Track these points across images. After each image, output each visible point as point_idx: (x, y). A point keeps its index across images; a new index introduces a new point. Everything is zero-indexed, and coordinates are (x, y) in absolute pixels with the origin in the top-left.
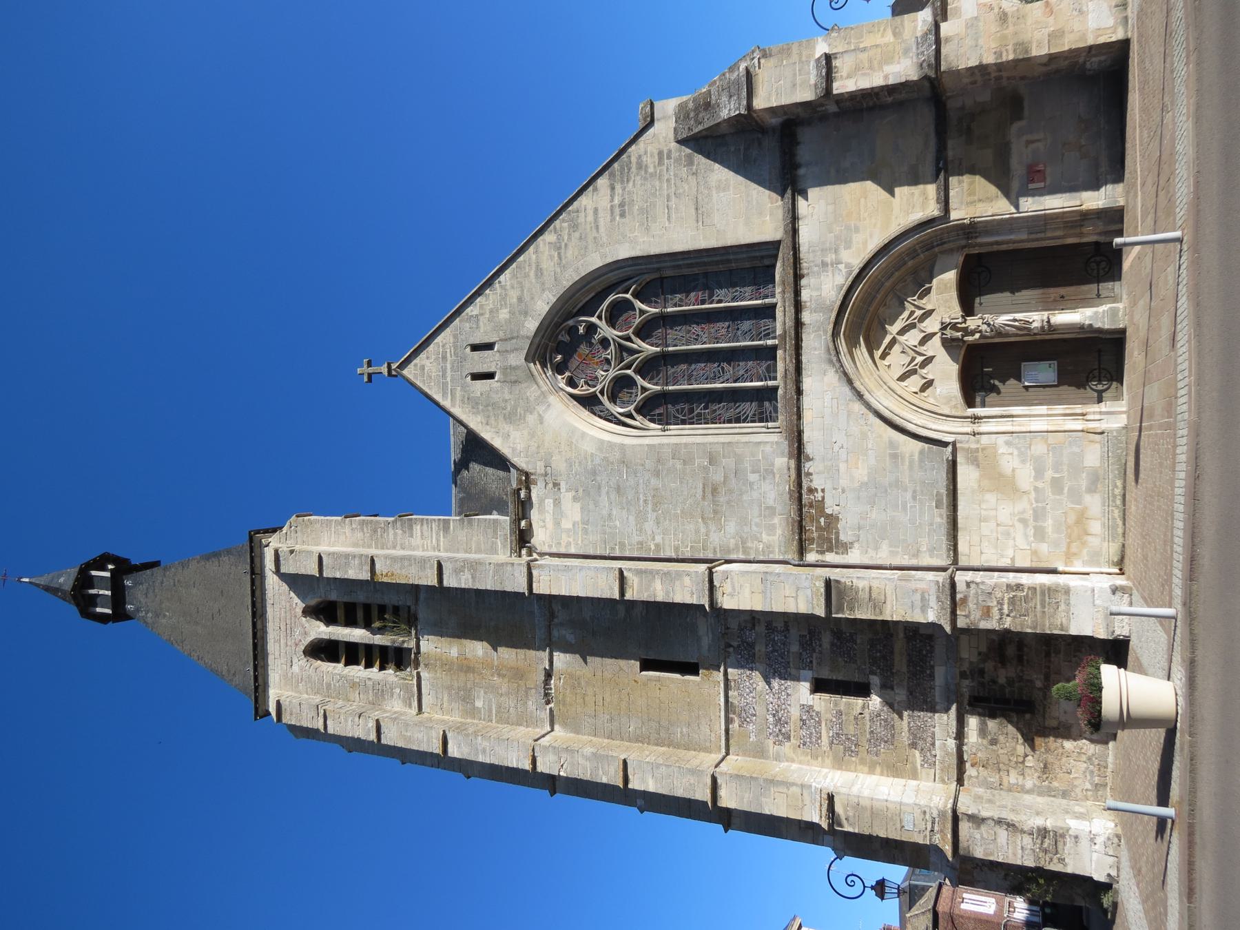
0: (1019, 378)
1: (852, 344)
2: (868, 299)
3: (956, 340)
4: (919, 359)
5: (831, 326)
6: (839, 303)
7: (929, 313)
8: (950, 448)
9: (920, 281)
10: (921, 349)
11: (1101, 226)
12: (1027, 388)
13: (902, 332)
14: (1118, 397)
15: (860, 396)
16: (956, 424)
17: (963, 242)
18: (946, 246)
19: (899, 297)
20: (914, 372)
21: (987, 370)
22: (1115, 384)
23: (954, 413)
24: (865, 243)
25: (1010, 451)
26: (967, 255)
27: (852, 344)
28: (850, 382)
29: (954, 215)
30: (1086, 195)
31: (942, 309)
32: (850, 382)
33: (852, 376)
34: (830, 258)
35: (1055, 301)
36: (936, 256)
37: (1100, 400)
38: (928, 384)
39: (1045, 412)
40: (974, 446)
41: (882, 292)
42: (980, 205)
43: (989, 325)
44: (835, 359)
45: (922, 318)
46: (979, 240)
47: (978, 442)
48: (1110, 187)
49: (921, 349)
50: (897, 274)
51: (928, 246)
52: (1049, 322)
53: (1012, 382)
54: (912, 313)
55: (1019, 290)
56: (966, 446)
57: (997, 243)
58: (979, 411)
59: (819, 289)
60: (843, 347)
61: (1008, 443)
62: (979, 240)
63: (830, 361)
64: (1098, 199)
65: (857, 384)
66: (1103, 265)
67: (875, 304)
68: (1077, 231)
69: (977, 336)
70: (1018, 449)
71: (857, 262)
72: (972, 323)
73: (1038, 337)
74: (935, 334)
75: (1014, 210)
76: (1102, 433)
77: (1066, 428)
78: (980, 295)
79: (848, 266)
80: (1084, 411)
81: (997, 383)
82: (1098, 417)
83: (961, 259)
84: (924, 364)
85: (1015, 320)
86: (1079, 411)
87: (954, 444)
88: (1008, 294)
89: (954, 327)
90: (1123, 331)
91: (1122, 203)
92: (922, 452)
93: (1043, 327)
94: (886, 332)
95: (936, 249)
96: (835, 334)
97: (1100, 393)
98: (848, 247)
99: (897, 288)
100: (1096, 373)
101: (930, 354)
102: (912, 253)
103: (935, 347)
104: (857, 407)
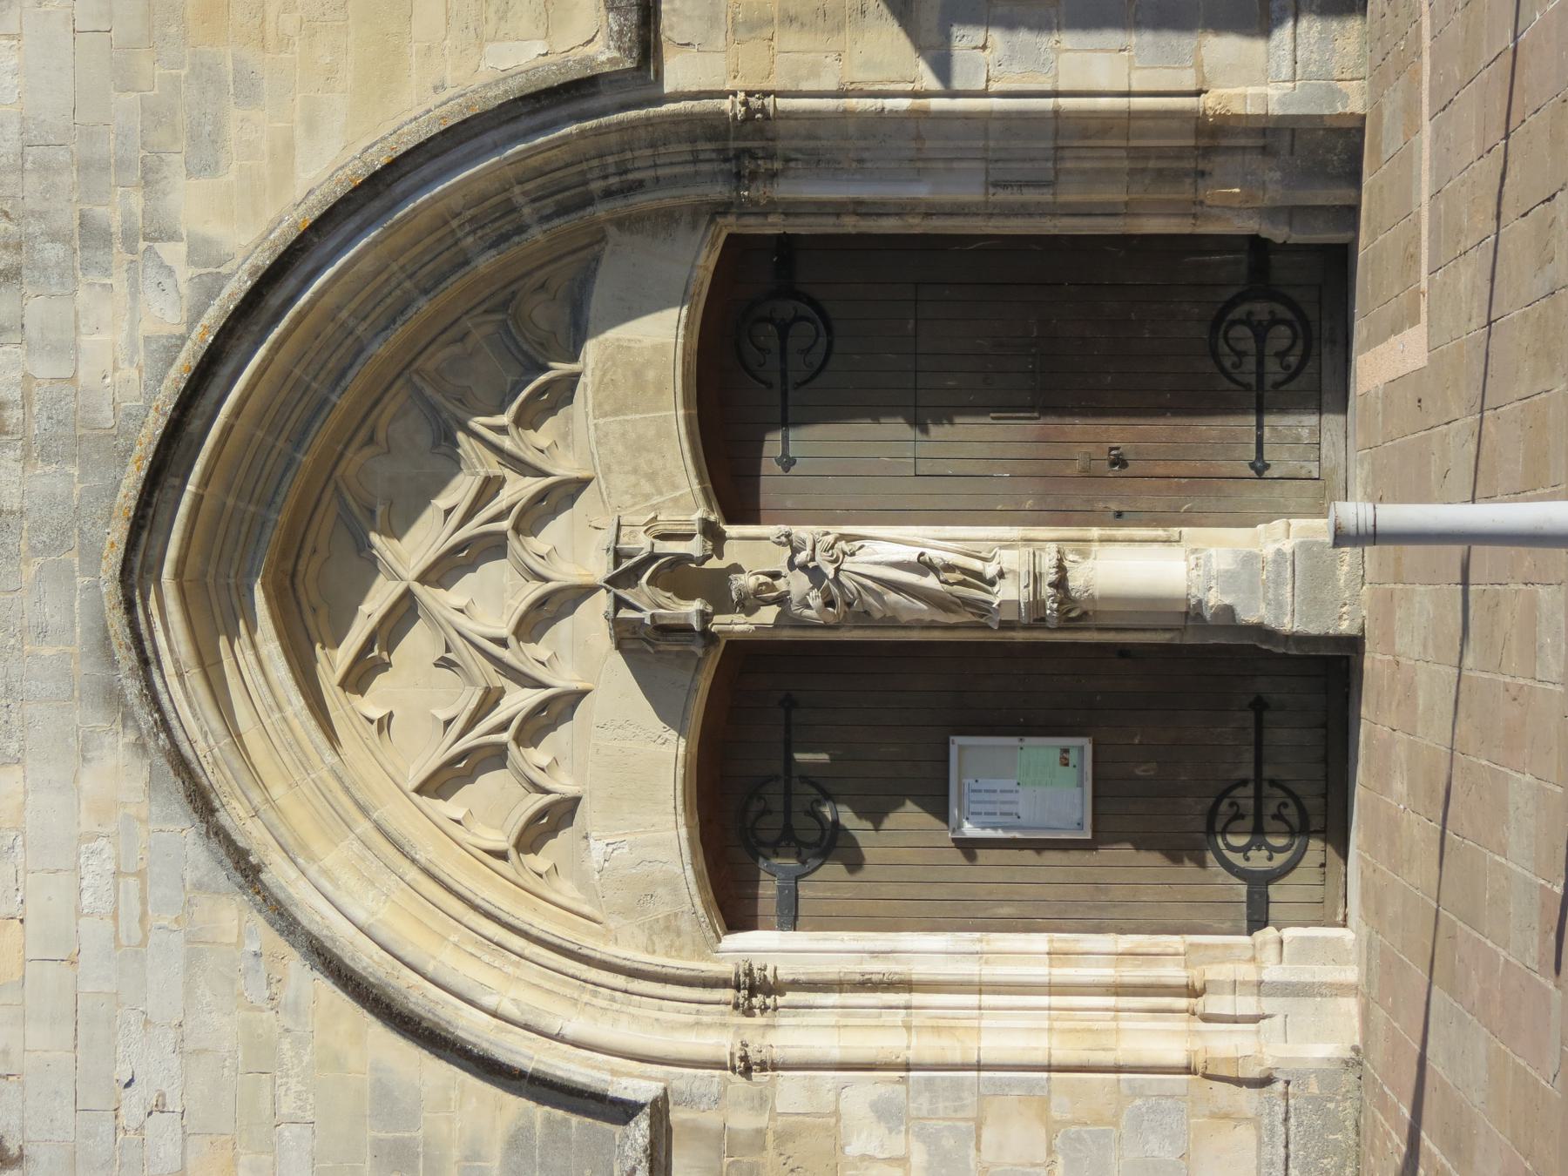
0: (938, 804)
1: (215, 618)
2: (293, 411)
3: (677, 631)
4: (518, 701)
5: (118, 532)
6: (154, 427)
7: (560, 496)
8: (640, 1129)
9: (529, 346)
10: (526, 656)
11: (1274, 187)
12: (969, 847)
13: (444, 570)
14: (1328, 912)
15: (247, 870)
16: (670, 1012)
17: (719, 191)
18: (643, 202)
19: (434, 410)
20: (494, 757)
21: (800, 755)
22: (1315, 845)
23: (658, 960)
24: (285, 152)
25: (897, 1145)
26: (731, 237)
27: (215, 618)
28: (201, 802)
29: (682, 71)
30: (1222, 50)
31: (620, 481)
32: (201, 802)
33: (211, 776)
34: (119, 207)
35: (1088, 475)
36: (602, 238)
37: (1257, 919)
38: (555, 817)
39: (1039, 971)
40: (743, 1121)
41: (357, 380)
42: (790, 40)
43: (815, 574)
44: (132, 688)
45: (536, 513)
46: (784, 190)
47: (762, 1102)
48: (1310, 27)
49: (526, 656)
50: (424, 306)
51: (565, 191)
52: (1061, 584)
53: (909, 817)
54: (490, 487)
55: (945, 414)
56: (711, 1119)
57: (859, 208)
58: (764, 947)
59: (68, 349)
60: (172, 638)
61: (886, 1113)
62: (784, 190)
63: (112, 697)
64: (1266, 77)
65: (235, 814)
66: (1281, 337)
67: (319, 439)
68: (1185, 192)
69: (768, 615)
70: (930, 1140)
71: (247, 244)
72: (753, 551)
73: (1019, 636)
74: (587, 591)
75: (930, 82)
76: (1265, 1082)
77: (1125, 1051)
78: (785, 423)
79: (200, 251)
80: (1195, 976)
81: (847, 818)
82: (1247, 1004)
83: (708, 260)
84: (536, 726)
85: (924, 566)
86: (1173, 973)
87: (659, 1109)
88: (896, 429)
89: (676, 575)
90: (1352, 646)
91: (1356, 105)
92: (518, 1141)
93: (1036, 604)
94: (370, 566)
95: (601, 211)
96: (135, 574)
97: (1259, 883)
98: (204, 165)
99: (429, 363)
100: (1245, 796)
101: (564, 679)
102: (496, 217)
103: (583, 652)
104: (233, 918)
